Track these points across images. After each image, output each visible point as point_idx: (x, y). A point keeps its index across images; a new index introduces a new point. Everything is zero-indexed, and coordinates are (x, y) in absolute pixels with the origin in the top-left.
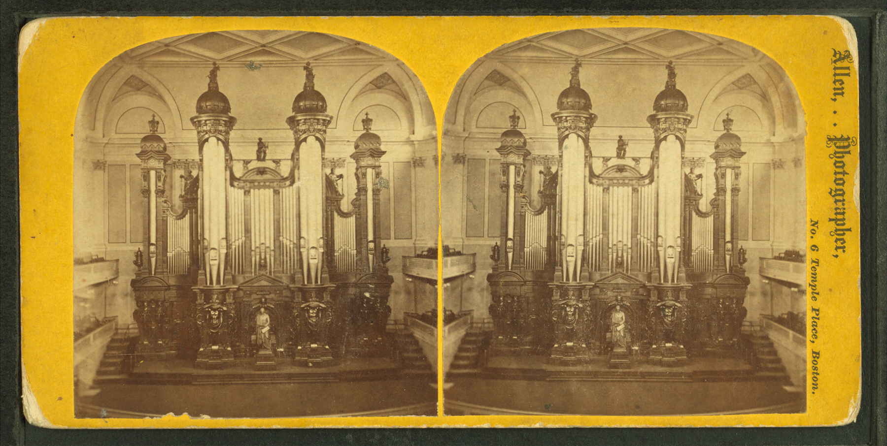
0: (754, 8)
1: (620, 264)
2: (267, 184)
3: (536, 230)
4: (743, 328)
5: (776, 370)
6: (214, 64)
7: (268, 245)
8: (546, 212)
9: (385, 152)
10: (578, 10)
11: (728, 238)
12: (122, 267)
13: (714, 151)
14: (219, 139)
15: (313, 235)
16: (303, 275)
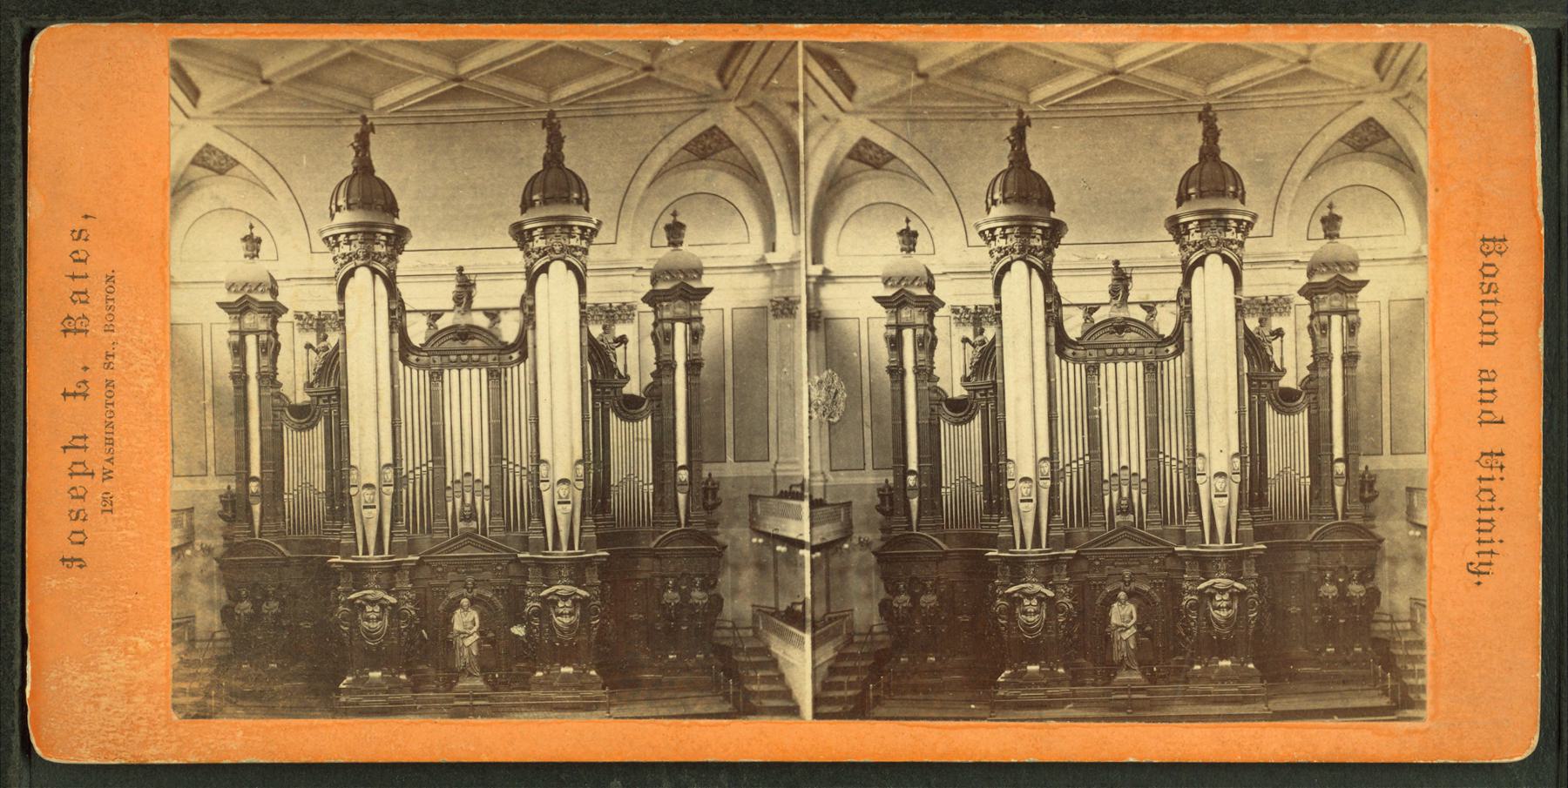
0: (1494, 12)
7: (477, 476)
10: (1031, 15)
12: (858, 516)
14: (375, 272)
15: (1219, 444)
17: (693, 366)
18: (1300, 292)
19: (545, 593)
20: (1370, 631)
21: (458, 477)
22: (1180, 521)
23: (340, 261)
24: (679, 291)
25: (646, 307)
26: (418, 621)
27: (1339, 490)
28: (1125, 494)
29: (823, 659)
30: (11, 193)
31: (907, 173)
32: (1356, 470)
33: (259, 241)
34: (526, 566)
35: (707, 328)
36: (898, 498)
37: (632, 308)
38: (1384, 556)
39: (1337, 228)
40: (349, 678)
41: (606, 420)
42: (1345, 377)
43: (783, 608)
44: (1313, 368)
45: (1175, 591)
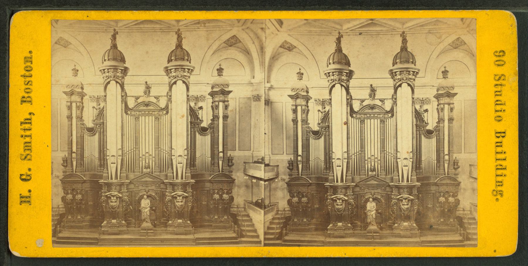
2: (376, 115)
3: (92, 144)
4: (458, 213)
5: (252, 237)
7: (376, 156)
10: (356, 7)
11: (221, 149)
13: (436, 93)
14: (342, 85)
18: (209, 94)
19: (173, 194)
20: (230, 211)
22: (391, 174)
23: (330, 82)
24: (221, 92)
26: (129, 203)
27: (221, 163)
29: (268, 219)
30: (5, 67)
31: (301, 53)
32: (227, 155)
33: (303, 74)
34: (166, 185)
35: (230, 105)
36: (295, 164)
37: (204, 97)
38: (235, 185)
39: (447, 75)
40: (331, 225)
41: (420, 138)
42: (223, 123)
43: (254, 201)
44: (213, 120)
45: (389, 198)
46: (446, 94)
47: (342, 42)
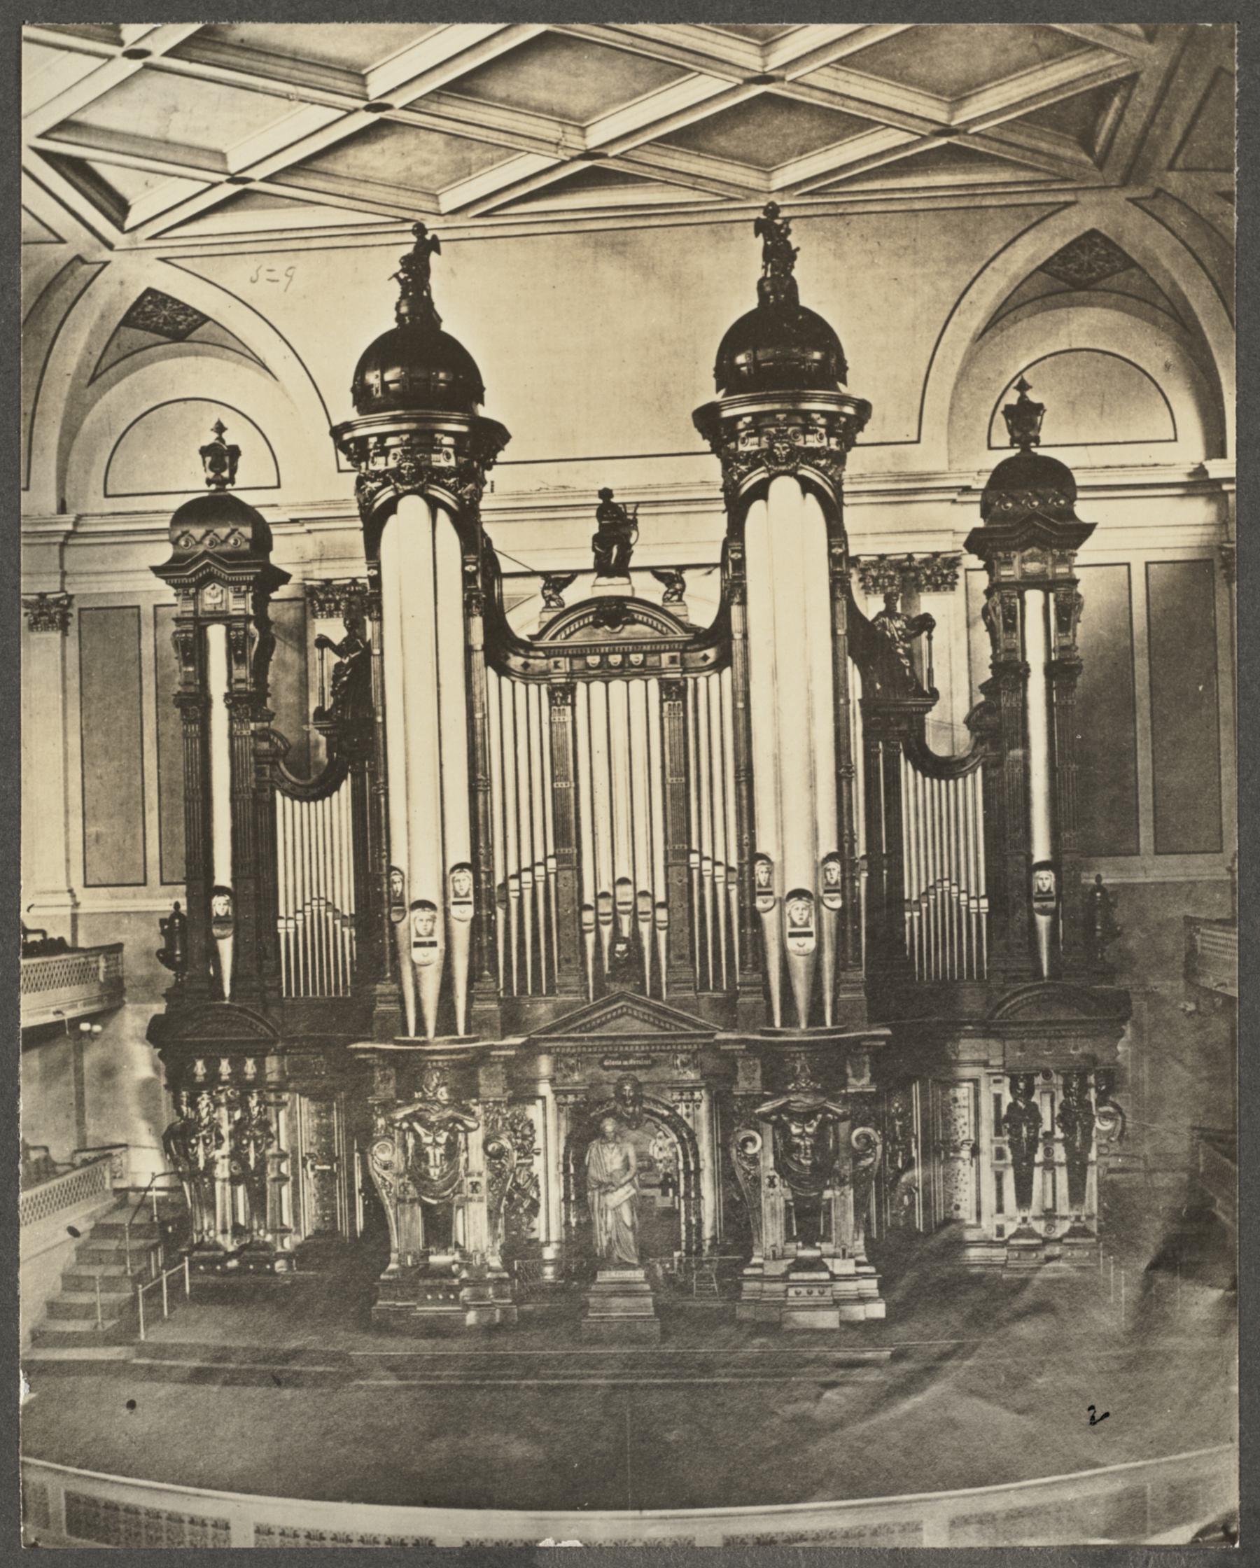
1: (629, 963)
6: (420, 230)
7: (643, 885)
8: (346, 787)
9: (1089, 529)
14: (434, 505)
15: (798, 831)
16: (768, 995)
17: (1060, 671)
21: (605, 886)
25: (972, 561)
28: (626, 931)
46: (1031, 509)
47: (435, 281)
